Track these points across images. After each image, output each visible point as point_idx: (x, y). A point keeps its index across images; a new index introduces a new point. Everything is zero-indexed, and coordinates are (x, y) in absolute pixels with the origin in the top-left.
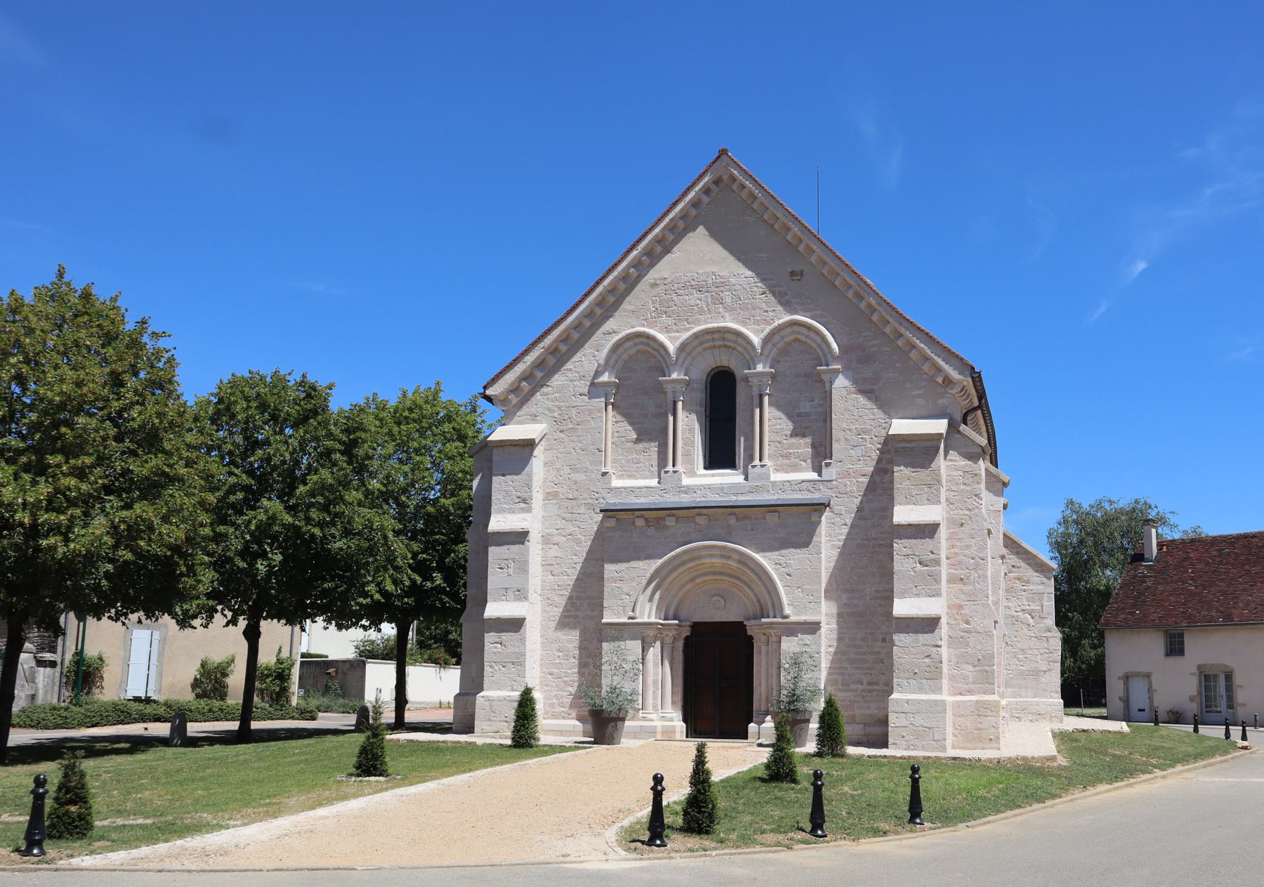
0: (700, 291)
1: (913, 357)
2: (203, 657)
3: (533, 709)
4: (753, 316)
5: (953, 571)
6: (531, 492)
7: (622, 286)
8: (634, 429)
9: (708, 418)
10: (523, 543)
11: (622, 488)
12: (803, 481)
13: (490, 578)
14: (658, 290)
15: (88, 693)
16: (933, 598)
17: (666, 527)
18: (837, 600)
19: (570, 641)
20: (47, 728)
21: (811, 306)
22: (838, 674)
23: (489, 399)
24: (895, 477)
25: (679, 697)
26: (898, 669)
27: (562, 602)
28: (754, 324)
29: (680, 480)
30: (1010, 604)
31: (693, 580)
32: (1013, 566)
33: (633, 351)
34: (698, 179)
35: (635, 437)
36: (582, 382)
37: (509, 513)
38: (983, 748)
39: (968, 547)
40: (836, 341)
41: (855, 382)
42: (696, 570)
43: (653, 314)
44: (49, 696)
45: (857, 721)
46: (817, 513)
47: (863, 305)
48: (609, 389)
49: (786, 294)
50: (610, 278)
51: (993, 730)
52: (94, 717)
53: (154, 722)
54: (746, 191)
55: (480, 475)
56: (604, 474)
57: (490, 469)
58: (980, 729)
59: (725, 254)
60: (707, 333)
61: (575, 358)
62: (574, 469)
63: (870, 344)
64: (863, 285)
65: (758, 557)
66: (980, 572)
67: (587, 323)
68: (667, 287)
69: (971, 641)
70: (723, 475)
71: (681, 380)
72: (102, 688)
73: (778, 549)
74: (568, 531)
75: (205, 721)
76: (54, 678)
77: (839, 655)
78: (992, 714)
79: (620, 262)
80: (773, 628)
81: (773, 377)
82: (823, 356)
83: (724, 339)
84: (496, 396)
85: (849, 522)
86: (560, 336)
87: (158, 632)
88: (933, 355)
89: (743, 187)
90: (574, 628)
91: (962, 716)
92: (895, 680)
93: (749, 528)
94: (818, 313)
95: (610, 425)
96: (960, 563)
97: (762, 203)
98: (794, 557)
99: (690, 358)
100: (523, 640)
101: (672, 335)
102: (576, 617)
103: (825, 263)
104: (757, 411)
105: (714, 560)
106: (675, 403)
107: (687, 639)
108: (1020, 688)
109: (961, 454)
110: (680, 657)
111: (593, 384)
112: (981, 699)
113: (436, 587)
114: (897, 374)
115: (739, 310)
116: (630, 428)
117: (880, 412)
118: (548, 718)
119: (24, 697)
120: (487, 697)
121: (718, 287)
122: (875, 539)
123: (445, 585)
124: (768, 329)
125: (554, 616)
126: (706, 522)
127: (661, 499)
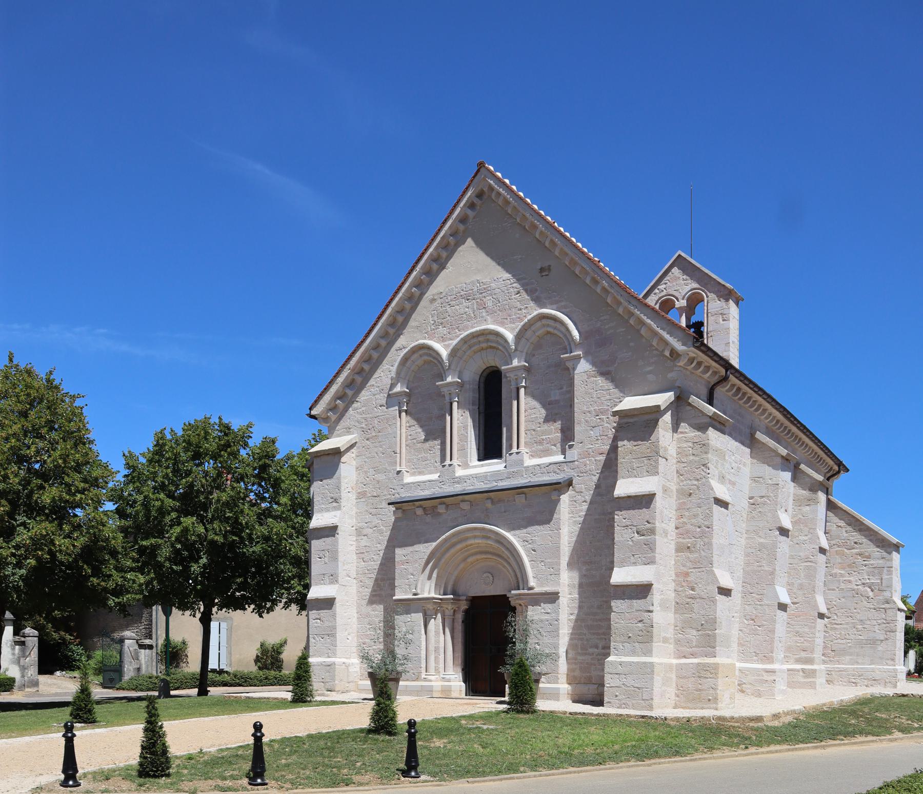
1: (644, 334)
2: (262, 641)
4: (510, 316)
5: (681, 540)
6: (340, 493)
7: (408, 306)
8: (423, 431)
10: (334, 536)
11: (411, 483)
12: (550, 464)
14: (436, 304)
15: (177, 666)
16: (648, 566)
17: (439, 514)
18: (580, 570)
19: (377, 616)
20: (142, 690)
21: (557, 298)
23: (313, 417)
25: (459, 661)
26: (615, 633)
27: (370, 583)
28: (511, 323)
31: (465, 559)
32: (856, 543)
33: (420, 362)
35: (424, 437)
36: (382, 395)
37: (326, 511)
38: (702, 708)
39: (695, 516)
40: (577, 329)
41: (593, 364)
42: (466, 551)
44: (150, 669)
45: (594, 682)
46: (556, 493)
47: (598, 290)
48: (401, 398)
49: (536, 290)
50: (397, 299)
51: (711, 691)
52: (176, 683)
53: (223, 686)
54: (501, 198)
56: (399, 472)
58: (700, 690)
60: (474, 337)
61: (375, 376)
62: (377, 471)
63: (607, 327)
65: (508, 535)
66: (706, 540)
69: (696, 606)
70: (489, 465)
71: (454, 382)
72: (188, 663)
73: (526, 527)
75: (262, 686)
76: (152, 657)
77: (579, 623)
78: (711, 676)
79: (403, 283)
80: (520, 599)
81: (527, 370)
82: (566, 344)
85: (588, 498)
86: (361, 357)
87: (226, 624)
88: (658, 330)
89: (499, 194)
90: (380, 603)
91: (684, 677)
92: (612, 644)
93: (503, 510)
94: (563, 304)
95: (404, 430)
96: (688, 532)
98: (538, 532)
100: (334, 616)
102: (379, 595)
103: (567, 254)
104: (515, 403)
105: (477, 541)
106: (451, 404)
107: (467, 612)
108: (857, 656)
109: (691, 425)
110: (459, 627)
111: (389, 395)
112: (702, 662)
114: (630, 354)
115: (498, 312)
116: (420, 430)
117: (616, 390)
118: (363, 680)
119: (132, 670)
121: (482, 293)
125: (365, 596)
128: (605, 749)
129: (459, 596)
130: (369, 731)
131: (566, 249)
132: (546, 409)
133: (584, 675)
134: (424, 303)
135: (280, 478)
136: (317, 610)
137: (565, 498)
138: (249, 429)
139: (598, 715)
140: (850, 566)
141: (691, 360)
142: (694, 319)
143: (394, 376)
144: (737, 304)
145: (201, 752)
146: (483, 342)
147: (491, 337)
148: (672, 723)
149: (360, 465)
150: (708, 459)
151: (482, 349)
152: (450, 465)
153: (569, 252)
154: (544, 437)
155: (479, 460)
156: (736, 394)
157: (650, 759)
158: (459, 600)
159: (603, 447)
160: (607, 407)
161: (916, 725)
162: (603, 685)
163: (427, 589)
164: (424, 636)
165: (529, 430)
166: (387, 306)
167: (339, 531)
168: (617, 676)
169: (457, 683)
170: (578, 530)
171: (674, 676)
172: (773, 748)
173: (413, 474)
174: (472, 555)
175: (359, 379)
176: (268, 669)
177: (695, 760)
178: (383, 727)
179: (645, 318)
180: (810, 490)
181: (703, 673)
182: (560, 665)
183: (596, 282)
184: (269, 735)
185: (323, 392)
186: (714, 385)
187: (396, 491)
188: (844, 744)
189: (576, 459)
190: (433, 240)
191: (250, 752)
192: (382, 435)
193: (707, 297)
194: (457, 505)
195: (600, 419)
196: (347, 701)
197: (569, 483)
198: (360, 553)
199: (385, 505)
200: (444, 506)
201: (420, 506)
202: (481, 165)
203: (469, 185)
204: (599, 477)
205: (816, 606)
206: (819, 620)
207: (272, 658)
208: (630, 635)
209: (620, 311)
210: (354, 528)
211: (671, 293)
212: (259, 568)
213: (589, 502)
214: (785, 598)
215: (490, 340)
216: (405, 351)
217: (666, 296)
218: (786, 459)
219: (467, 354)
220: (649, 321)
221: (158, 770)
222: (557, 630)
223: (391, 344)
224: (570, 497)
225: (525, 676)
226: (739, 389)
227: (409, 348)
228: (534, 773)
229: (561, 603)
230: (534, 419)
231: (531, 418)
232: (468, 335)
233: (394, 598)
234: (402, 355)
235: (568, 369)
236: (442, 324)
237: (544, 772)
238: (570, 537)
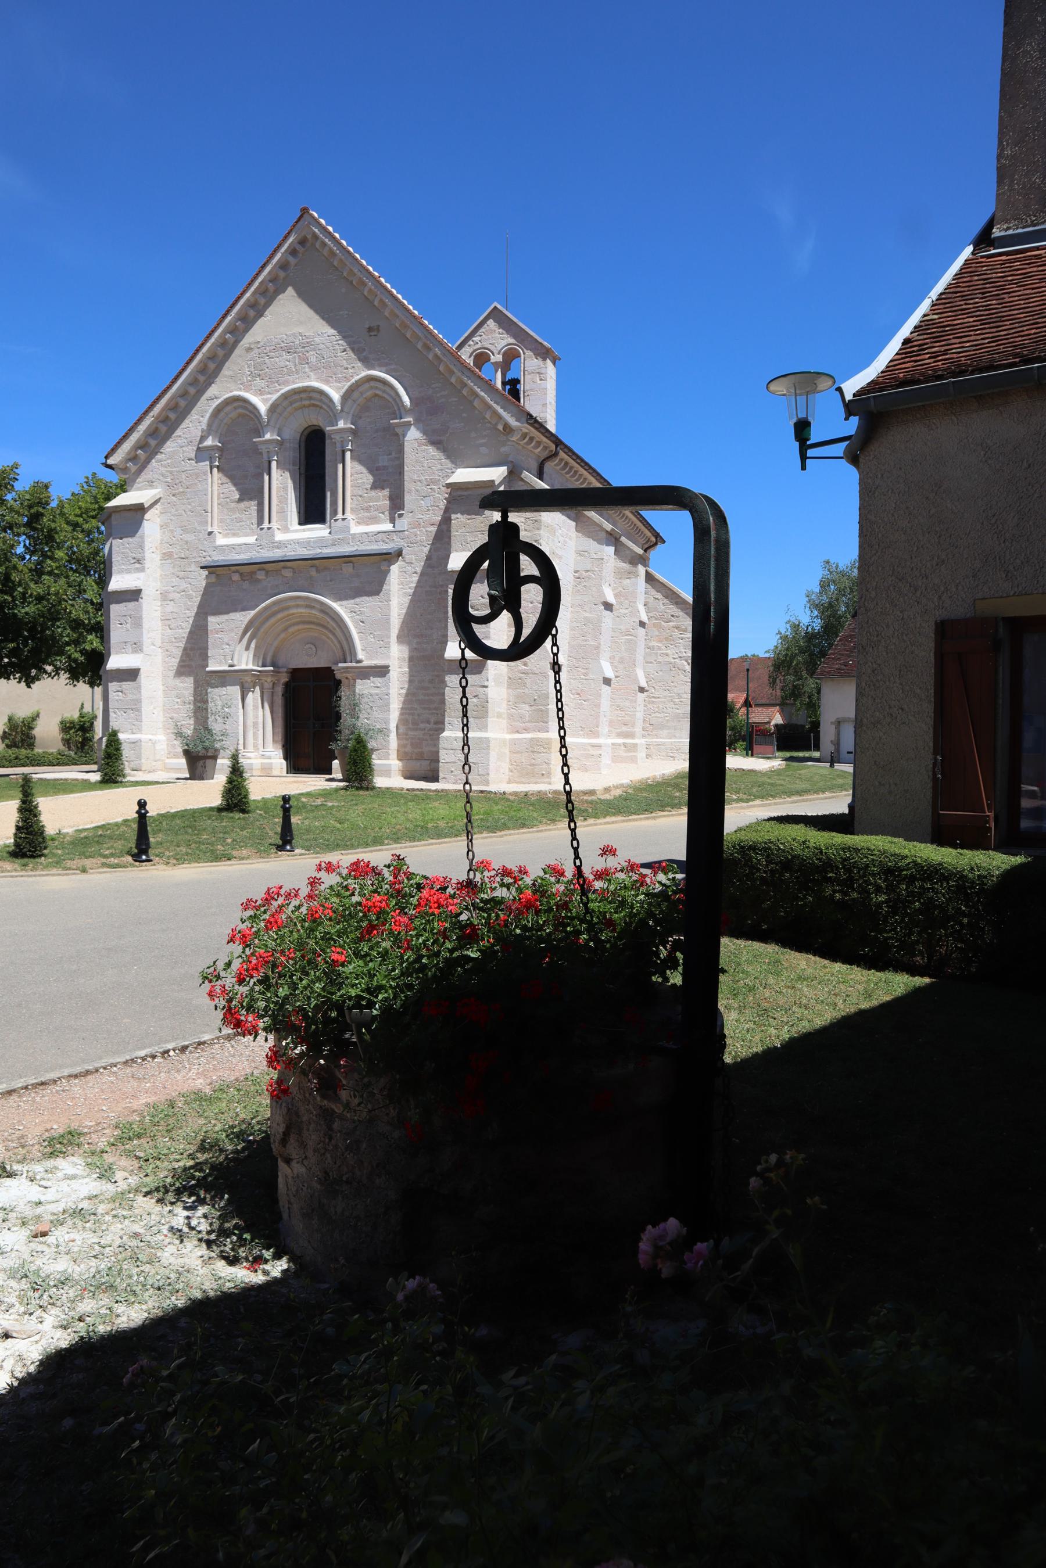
7: (221, 353)
8: (237, 490)
9: (303, 476)
10: (137, 600)
12: (379, 533)
14: (252, 354)
17: (258, 581)
18: (409, 643)
19: (186, 689)
21: (386, 361)
22: (409, 714)
23: (110, 467)
24: (452, 525)
25: (280, 737)
27: (178, 653)
28: (336, 381)
29: (273, 536)
30: (668, 652)
31: (286, 629)
32: (672, 616)
33: (234, 415)
34: (283, 240)
35: (238, 497)
38: (536, 783)
40: (408, 394)
41: (425, 433)
42: (287, 620)
46: (385, 563)
47: (431, 356)
49: (364, 350)
51: (545, 766)
54: (327, 249)
56: (210, 533)
58: (533, 765)
59: (311, 313)
61: (183, 426)
62: (185, 531)
63: (438, 395)
64: (429, 336)
65: (335, 606)
68: (260, 350)
69: (528, 681)
70: (313, 530)
71: (274, 440)
73: (353, 598)
74: (182, 588)
75: (12, 767)
80: (348, 672)
82: (395, 408)
85: (419, 570)
86: (167, 404)
88: (492, 403)
89: (324, 244)
90: (190, 675)
91: (518, 752)
92: (447, 719)
93: (328, 579)
94: (393, 367)
95: (215, 488)
97: (341, 260)
98: (366, 603)
100: (139, 688)
101: (265, 397)
102: (189, 666)
103: (398, 316)
104: (340, 466)
106: (270, 463)
107: (287, 685)
110: (279, 700)
111: (199, 449)
112: (535, 736)
114: (462, 424)
116: (234, 489)
117: (447, 461)
125: (172, 666)
127: (258, 555)
128: (456, 822)
129: (278, 667)
130: (220, 809)
131: (397, 312)
132: (373, 475)
133: (416, 751)
134: (238, 351)
135: (55, 529)
137: (395, 569)
138: (15, 470)
139: (436, 791)
140: (667, 639)
141: (524, 436)
142: (510, 376)
143: (205, 428)
144: (554, 364)
145: (59, 833)
146: (305, 399)
147: (314, 395)
148: (512, 798)
150: (540, 535)
152: (269, 528)
153: (400, 314)
154: (371, 504)
155: (300, 524)
156: (563, 468)
157: (500, 831)
158: (279, 672)
161: (734, 797)
162: (438, 761)
163: (244, 660)
164: (241, 710)
166: (198, 351)
167: (143, 594)
168: (452, 751)
169: (277, 760)
171: (507, 752)
172: (608, 819)
173: (226, 536)
174: (294, 624)
175: (163, 429)
176: (18, 747)
177: (541, 831)
178: (236, 805)
179: (478, 390)
180: (631, 563)
181: (536, 748)
182: (391, 741)
183: (427, 348)
184: (152, 810)
185: (121, 440)
186: (544, 460)
188: (672, 815)
190: (250, 284)
191: (135, 826)
193: (524, 354)
194: (278, 572)
196: (161, 781)
197: (399, 553)
198: (165, 620)
199: (193, 568)
200: (263, 572)
202: (305, 211)
203: (291, 230)
204: (430, 549)
205: (636, 680)
206: (640, 694)
207: (22, 734)
209: (453, 380)
210: (158, 592)
211: (486, 346)
212: (32, 630)
214: (609, 673)
215: (313, 398)
217: (481, 348)
218: (610, 534)
219: (288, 410)
220: (482, 394)
221: (36, 851)
222: (388, 705)
223: (201, 392)
224: (400, 567)
225: (364, 752)
226: (566, 464)
227: (222, 399)
228: (399, 845)
229: (391, 676)
232: (289, 391)
233: (207, 669)
234: (214, 406)
235: (397, 435)
236: (259, 375)
237: (408, 844)
238: (401, 609)
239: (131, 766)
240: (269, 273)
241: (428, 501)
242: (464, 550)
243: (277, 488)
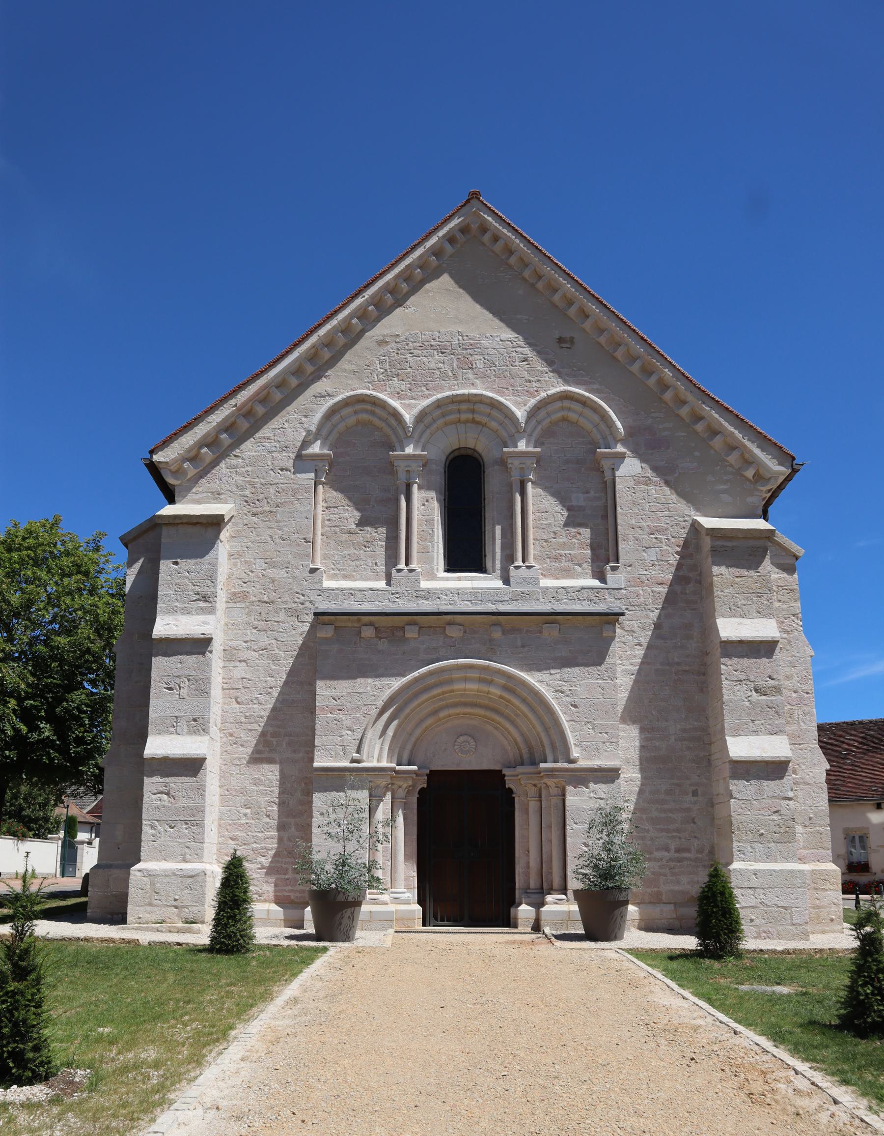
0: (442, 353)
3: (246, 891)
4: (511, 386)
6: (215, 587)
10: (203, 654)
11: (337, 589)
12: (583, 588)
13: (153, 703)
26: (739, 829)
28: (514, 394)
31: (435, 712)
33: (352, 420)
37: (183, 614)
42: (442, 700)
43: (381, 376)
47: (652, 381)
55: (141, 561)
56: (313, 571)
57: (158, 552)
58: (818, 907)
60: (453, 402)
62: (270, 563)
63: (661, 427)
65: (531, 678)
66: (805, 708)
67: (294, 382)
68: (399, 345)
70: (472, 579)
71: (420, 456)
74: (261, 644)
78: (831, 887)
80: (553, 777)
83: (473, 411)
84: (167, 463)
85: (645, 641)
86: (257, 393)
92: (735, 844)
93: (519, 643)
95: (319, 510)
99: (428, 431)
101: (407, 402)
111: (299, 457)
113: (44, 739)
114: (695, 464)
120: (147, 870)
122: (678, 664)
123: (55, 738)
124: (532, 402)
125: (240, 759)
126: (461, 634)
133: (649, 890)
136: (163, 776)
149: (238, 552)
151: (459, 421)
159: (663, 575)
160: (666, 526)
165: (538, 540)
168: (750, 891)
170: (631, 683)
173: (334, 577)
175: (244, 425)
182: (160, 863)
187: (307, 598)
189: (623, 586)
192: (283, 512)
195: (656, 538)
201: (371, 624)
204: (660, 615)
208: (762, 831)
213: (645, 646)
216: (330, 402)
220: (732, 429)
230: (545, 526)
231: (542, 524)
236: (398, 375)
239: (184, 915)
240: (420, 257)
241: (650, 555)
242: (734, 616)
243: (419, 520)
